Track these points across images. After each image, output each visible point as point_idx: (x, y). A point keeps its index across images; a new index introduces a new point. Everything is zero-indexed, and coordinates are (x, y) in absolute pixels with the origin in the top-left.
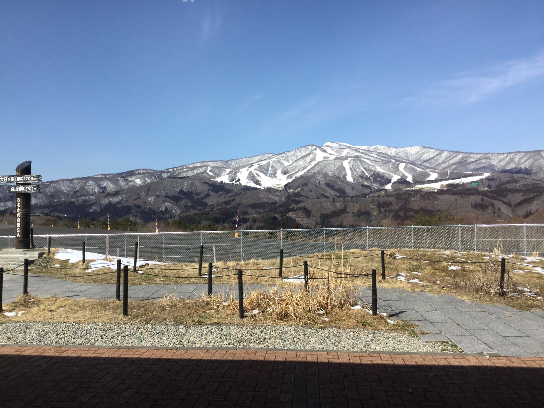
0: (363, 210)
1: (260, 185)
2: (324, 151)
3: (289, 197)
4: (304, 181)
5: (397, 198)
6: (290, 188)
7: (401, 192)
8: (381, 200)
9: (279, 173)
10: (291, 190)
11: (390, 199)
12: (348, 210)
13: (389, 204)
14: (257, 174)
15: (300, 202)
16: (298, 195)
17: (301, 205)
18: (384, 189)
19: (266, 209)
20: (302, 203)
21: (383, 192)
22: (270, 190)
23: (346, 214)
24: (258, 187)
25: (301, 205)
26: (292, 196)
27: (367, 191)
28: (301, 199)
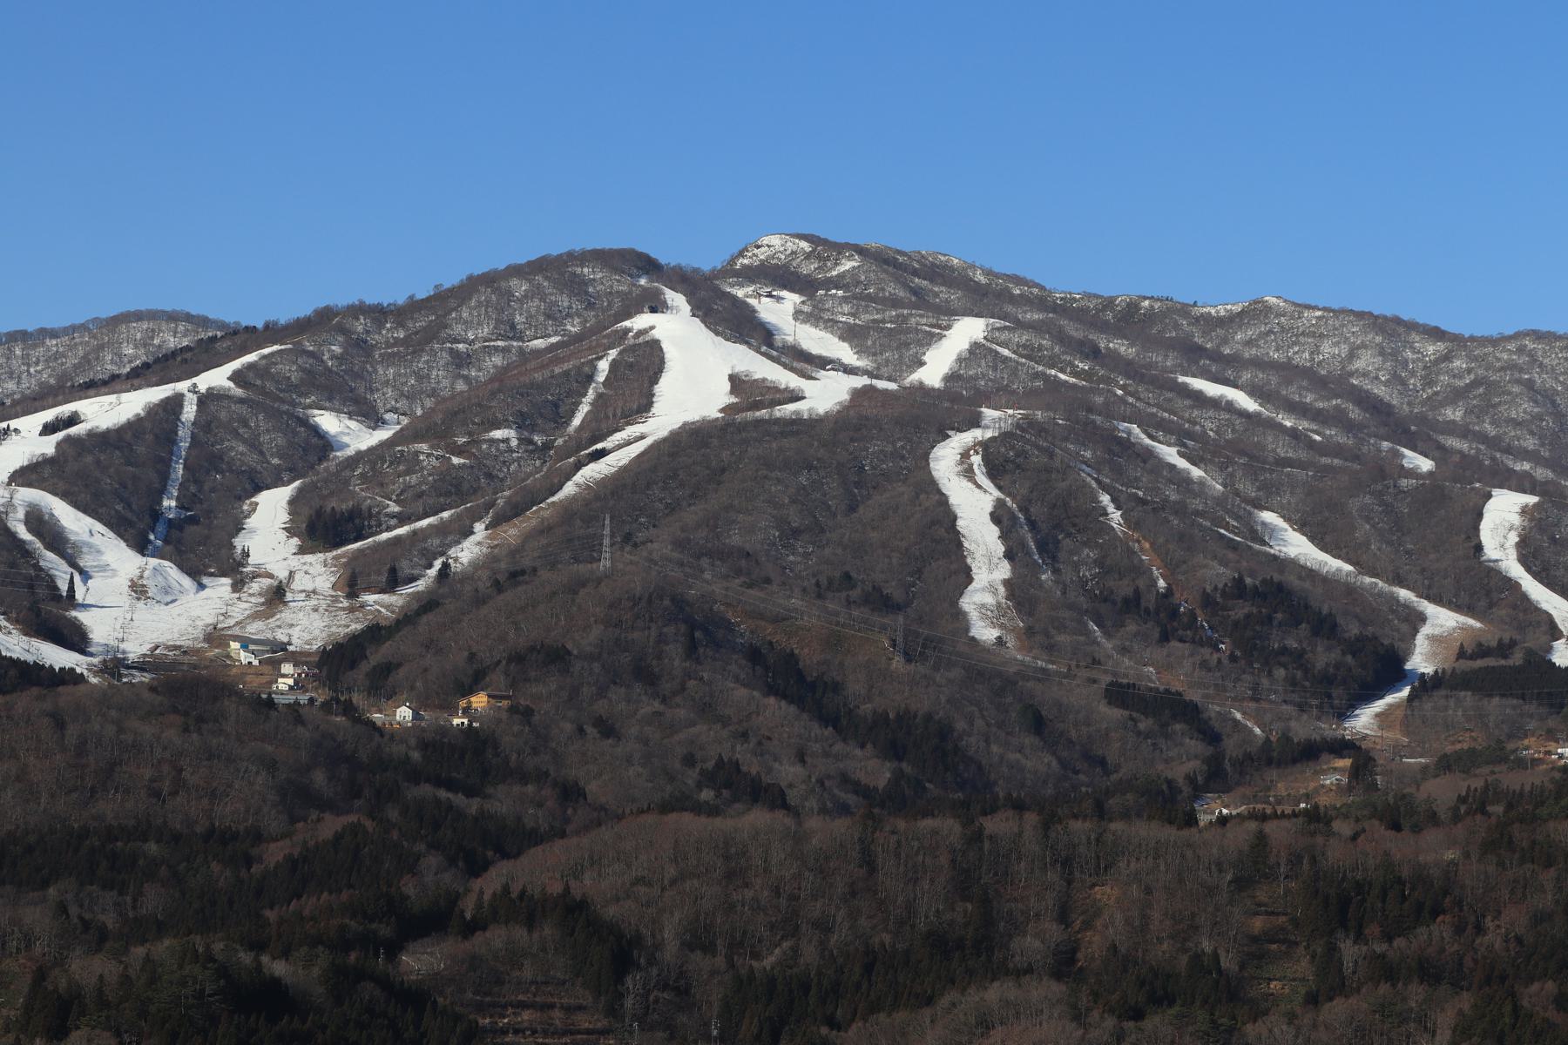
0: (1162, 951)
1: (75, 639)
2: (740, 325)
3: (366, 769)
4: (26, 634)
5: (1497, 843)
6: (383, 685)
7: (1513, 781)
8: (1353, 851)
9: (266, 528)
10: (404, 713)
11: (1437, 850)
12: (141, 604)
13: (1425, 898)
14: (38, 521)
15: (509, 840)
16: (465, 759)
17: (536, 871)
18: (1343, 747)
19: (153, 900)
20: (535, 855)
21: (1333, 775)
22: (188, 687)
23: (994, 993)
24: (57, 657)
25: (536, 871)
26: (415, 776)
27: (1182, 759)
28: (503, 801)
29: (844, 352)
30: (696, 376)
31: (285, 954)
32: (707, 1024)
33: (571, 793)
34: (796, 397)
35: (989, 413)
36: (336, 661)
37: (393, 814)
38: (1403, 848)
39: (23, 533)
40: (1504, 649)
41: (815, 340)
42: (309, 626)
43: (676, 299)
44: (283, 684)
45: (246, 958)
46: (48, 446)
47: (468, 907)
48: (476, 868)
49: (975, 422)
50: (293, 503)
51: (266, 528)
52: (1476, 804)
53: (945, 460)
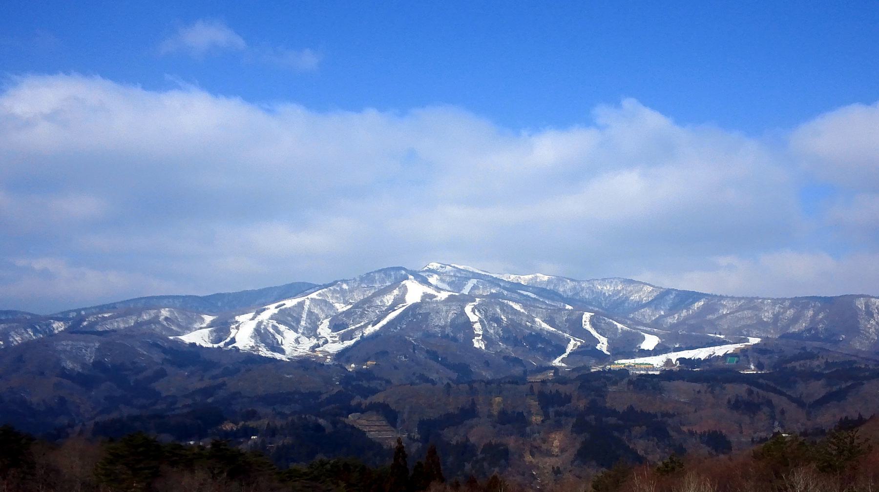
1: (282, 351)
2: (424, 281)
3: (348, 379)
6: (349, 361)
8: (551, 388)
15: (374, 392)
16: (367, 375)
24: (278, 356)
28: (374, 384)
29: (448, 288)
30: (414, 292)
31: (323, 417)
32: (211, 396)
33: (388, 382)
34: (435, 297)
35: (477, 300)
36: (340, 355)
37: (350, 387)
38: (562, 389)
39: (271, 330)
40: (587, 346)
41: (441, 285)
42: (334, 348)
43: (411, 277)
44: (328, 360)
45: (313, 418)
46: (276, 311)
47: (363, 406)
48: (366, 397)
49: (475, 301)
50: (330, 322)
51: (324, 330)
52: (578, 378)
53: (468, 309)
